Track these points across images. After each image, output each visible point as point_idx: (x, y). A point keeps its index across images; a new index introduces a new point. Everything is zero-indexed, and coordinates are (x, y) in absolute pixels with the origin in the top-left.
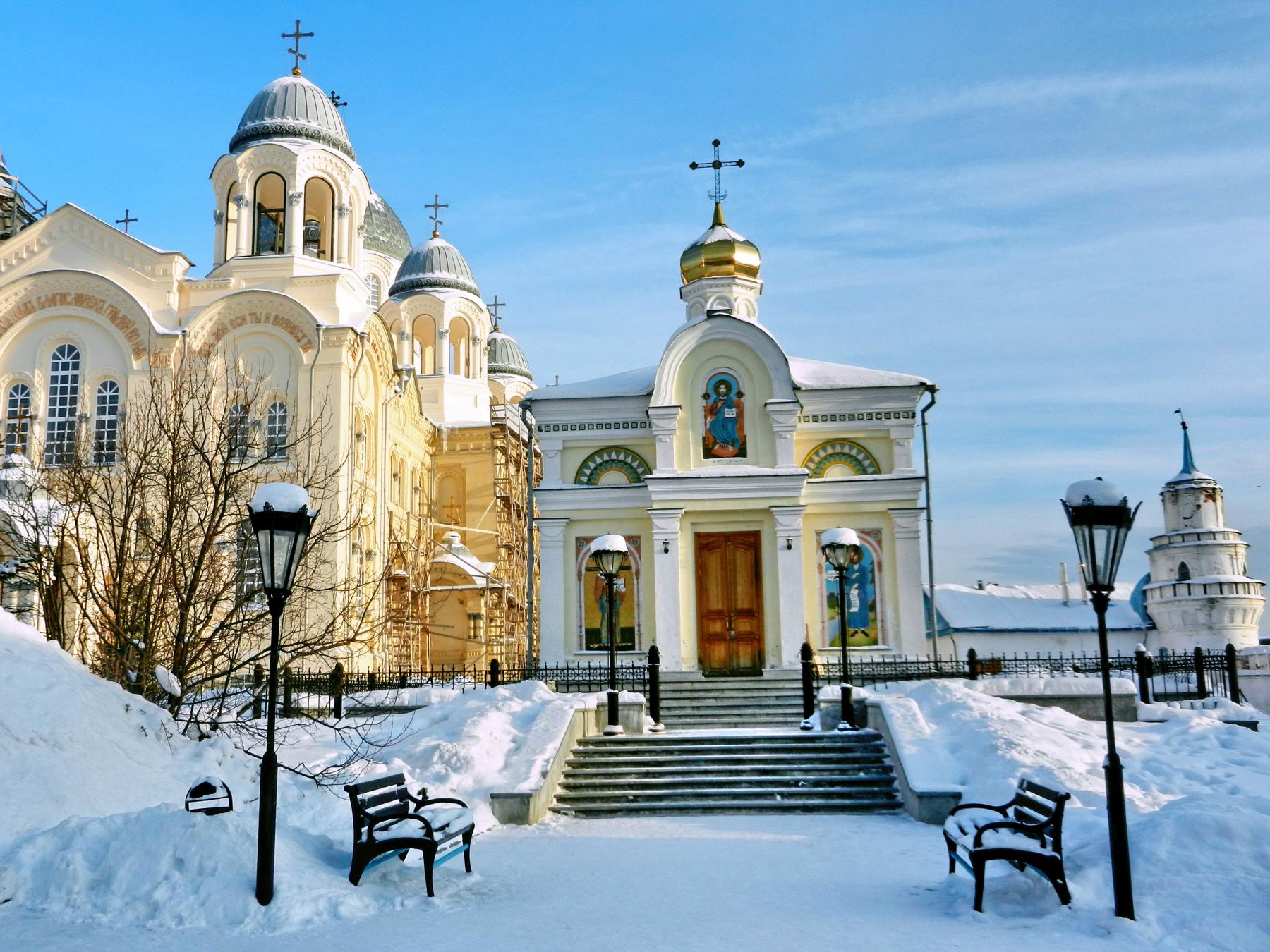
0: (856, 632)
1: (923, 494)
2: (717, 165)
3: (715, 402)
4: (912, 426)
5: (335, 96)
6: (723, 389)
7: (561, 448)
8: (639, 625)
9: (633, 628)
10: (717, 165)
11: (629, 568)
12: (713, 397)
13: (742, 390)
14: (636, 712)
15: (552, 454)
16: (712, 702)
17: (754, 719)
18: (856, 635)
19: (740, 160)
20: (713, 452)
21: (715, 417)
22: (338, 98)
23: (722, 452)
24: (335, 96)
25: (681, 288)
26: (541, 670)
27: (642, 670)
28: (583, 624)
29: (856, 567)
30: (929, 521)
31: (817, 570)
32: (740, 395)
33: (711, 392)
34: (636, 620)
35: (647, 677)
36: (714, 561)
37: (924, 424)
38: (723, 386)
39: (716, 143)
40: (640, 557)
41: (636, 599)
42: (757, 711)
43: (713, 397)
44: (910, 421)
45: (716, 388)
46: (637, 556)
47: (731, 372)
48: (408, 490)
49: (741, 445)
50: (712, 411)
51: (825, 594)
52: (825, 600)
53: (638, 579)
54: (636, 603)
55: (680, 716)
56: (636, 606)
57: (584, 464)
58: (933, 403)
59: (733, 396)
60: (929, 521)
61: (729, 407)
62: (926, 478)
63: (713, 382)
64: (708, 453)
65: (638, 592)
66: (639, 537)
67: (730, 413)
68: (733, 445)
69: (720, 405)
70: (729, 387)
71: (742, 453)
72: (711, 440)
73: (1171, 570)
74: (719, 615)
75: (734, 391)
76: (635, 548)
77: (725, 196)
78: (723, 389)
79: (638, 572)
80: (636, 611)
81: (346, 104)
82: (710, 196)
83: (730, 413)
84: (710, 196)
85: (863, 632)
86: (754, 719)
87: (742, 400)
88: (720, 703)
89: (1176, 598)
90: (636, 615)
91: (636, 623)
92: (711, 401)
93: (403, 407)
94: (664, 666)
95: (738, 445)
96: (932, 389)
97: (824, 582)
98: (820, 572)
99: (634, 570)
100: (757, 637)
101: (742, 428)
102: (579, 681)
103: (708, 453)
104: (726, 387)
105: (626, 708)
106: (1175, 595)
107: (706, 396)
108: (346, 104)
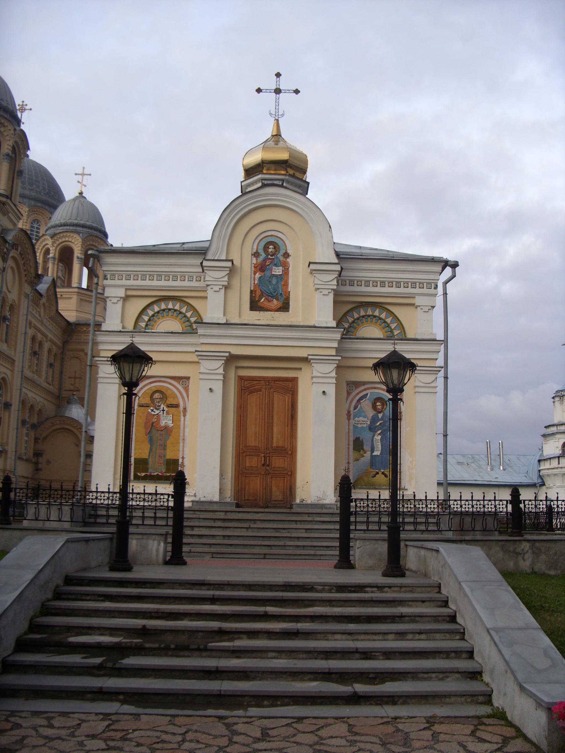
0: (378, 473)
1: (442, 354)
2: (278, 91)
3: (265, 260)
4: (435, 295)
5: (24, 104)
6: (271, 249)
7: (123, 295)
8: (183, 458)
9: (178, 460)
10: (278, 91)
11: (177, 406)
12: (263, 256)
13: (289, 251)
14: (156, 542)
15: (115, 300)
16: (244, 533)
17: (283, 552)
18: (377, 475)
19: (297, 90)
20: (259, 304)
21: (263, 274)
22: (26, 105)
23: (267, 305)
24: (24, 104)
25: (241, 182)
26: (91, 492)
27: (166, 497)
28: (20, 418)
29: (380, 416)
30: (446, 378)
31: (346, 417)
32: (286, 255)
33: (261, 251)
34: (181, 453)
35: (171, 504)
36: (253, 400)
37: (445, 294)
38: (271, 247)
39: (278, 75)
40: (188, 397)
41: (182, 434)
42: (288, 543)
43: (263, 256)
44: (432, 291)
45: (266, 248)
46: (185, 395)
47: (279, 235)
48: (45, 364)
49: (285, 299)
50: (261, 268)
51: (352, 439)
52: (351, 443)
53: (185, 416)
54: (181, 438)
55: (210, 545)
56: (181, 441)
57: (143, 311)
58: (454, 276)
59: (280, 256)
60: (446, 378)
61: (276, 265)
62: (445, 341)
63: (263, 244)
64: (255, 306)
65: (184, 428)
66: (188, 378)
67: (278, 271)
68: (277, 299)
69: (267, 263)
70: (276, 247)
71: (285, 307)
72: (258, 293)
73: (557, 447)
74: (256, 451)
75: (282, 252)
76: (184, 388)
77: (283, 115)
78: (271, 249)
79: (185, 409)
80: (181, 445)
81: (31, 109)
82: (271, 114)
83: (278, 271)
84: (271, 114)
85: (383, 473)
86: (283, 552)
87: (288, 260)
88: (250, 533)
89: (560, 466)
90: (181, 449)
91: (181, 456)
92: (261, 259)
93: (44, 304)
94: (25, 475)
95: (282, 299)
96: (455, 265)
97: (351, 428)
98: (349, 419)
99: (181, 408)
100: (290, 473)
101: (286, 285)
102: (108, 504)
103: (255, 306)
104: (275, 248)
105: (145, 537)
106: (559, 464)
107: (256, 254)
108: (31, 109)
